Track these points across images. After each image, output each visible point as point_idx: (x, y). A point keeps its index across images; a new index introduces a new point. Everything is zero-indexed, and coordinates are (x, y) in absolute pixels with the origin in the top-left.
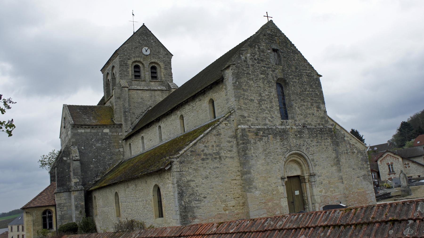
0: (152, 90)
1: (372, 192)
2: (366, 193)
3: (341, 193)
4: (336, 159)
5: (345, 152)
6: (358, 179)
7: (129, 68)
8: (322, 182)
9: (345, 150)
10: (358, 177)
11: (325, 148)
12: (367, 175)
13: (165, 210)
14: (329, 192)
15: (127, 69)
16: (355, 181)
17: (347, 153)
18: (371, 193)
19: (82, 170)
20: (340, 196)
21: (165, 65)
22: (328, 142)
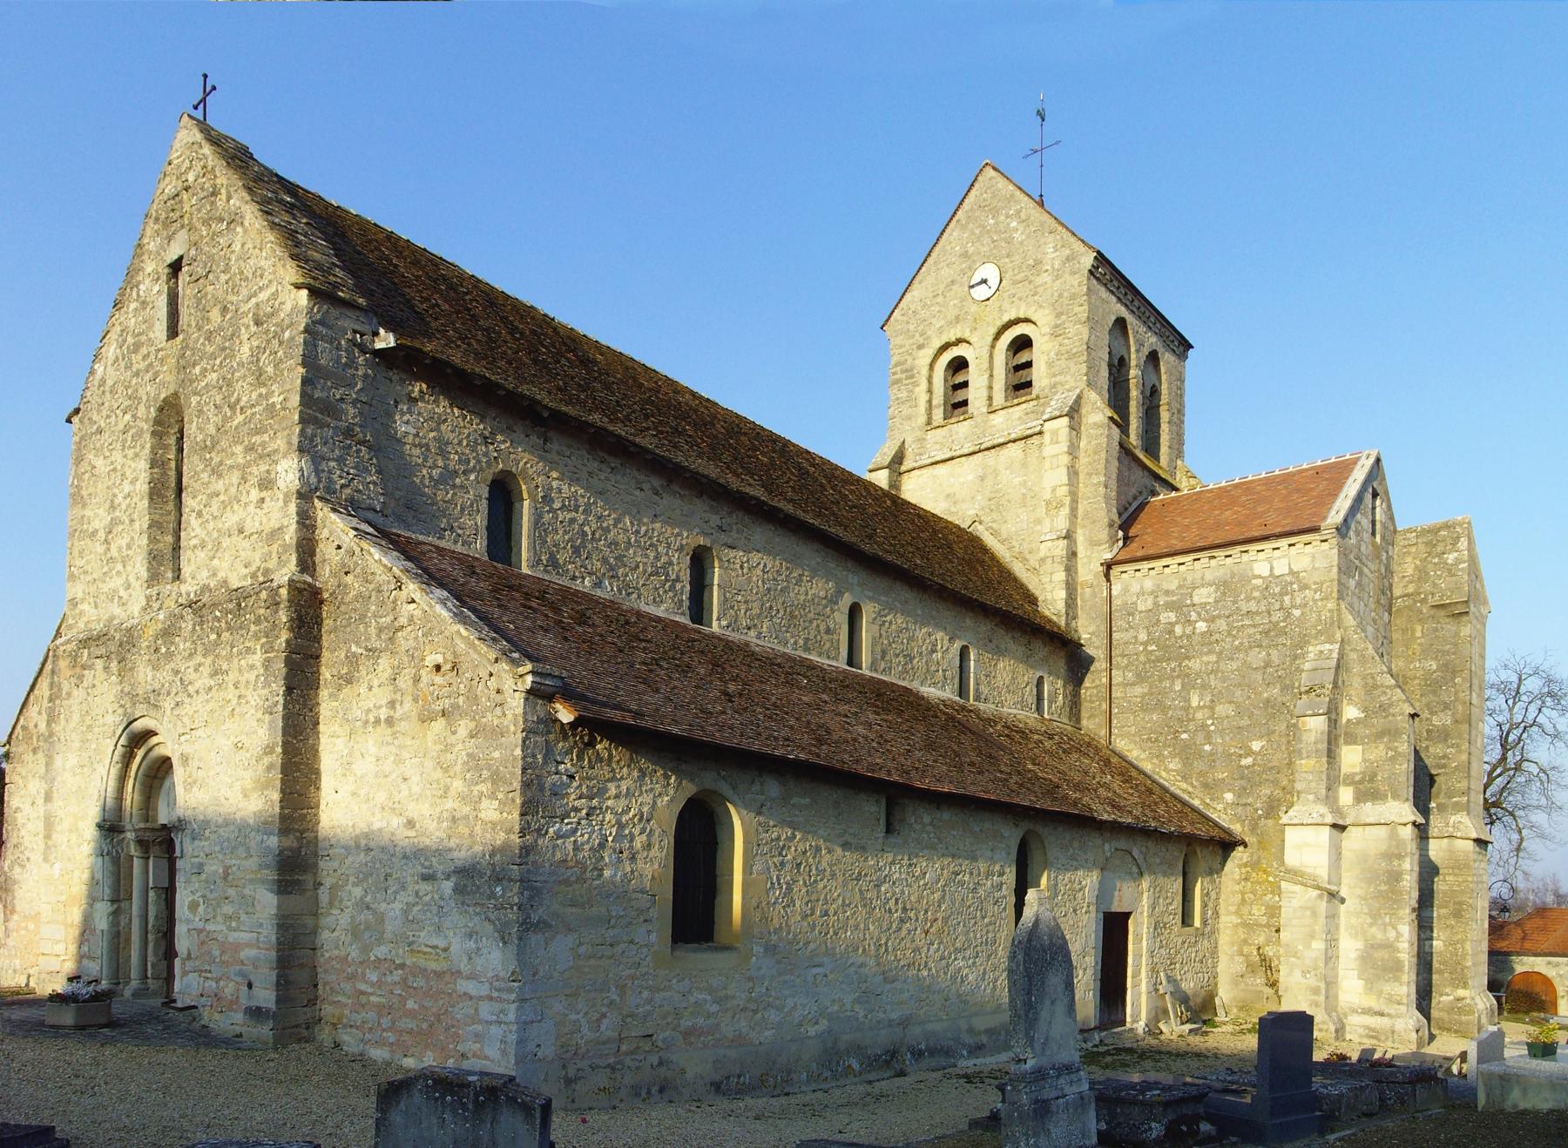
0: (987, 449)
1: (495, 994)
2: (455, 991)
3: (258, 939)
4: (266, 759)
5: (384, 713)
6: (425, 887)
7: (918, 385)
8: (201, 865)
9: (380, 707)
10: (426, 878)
11: (235, 701)
12: (481, 875)
13: (1439, 916)
14: (219, 919)
15: (912, 391)
16: (405, 897)
17: (390, 721)
18: (491, 998)
19: (1337, 737)
20: (253, 952)
21: (1058, 316)
22: (252, 667)
